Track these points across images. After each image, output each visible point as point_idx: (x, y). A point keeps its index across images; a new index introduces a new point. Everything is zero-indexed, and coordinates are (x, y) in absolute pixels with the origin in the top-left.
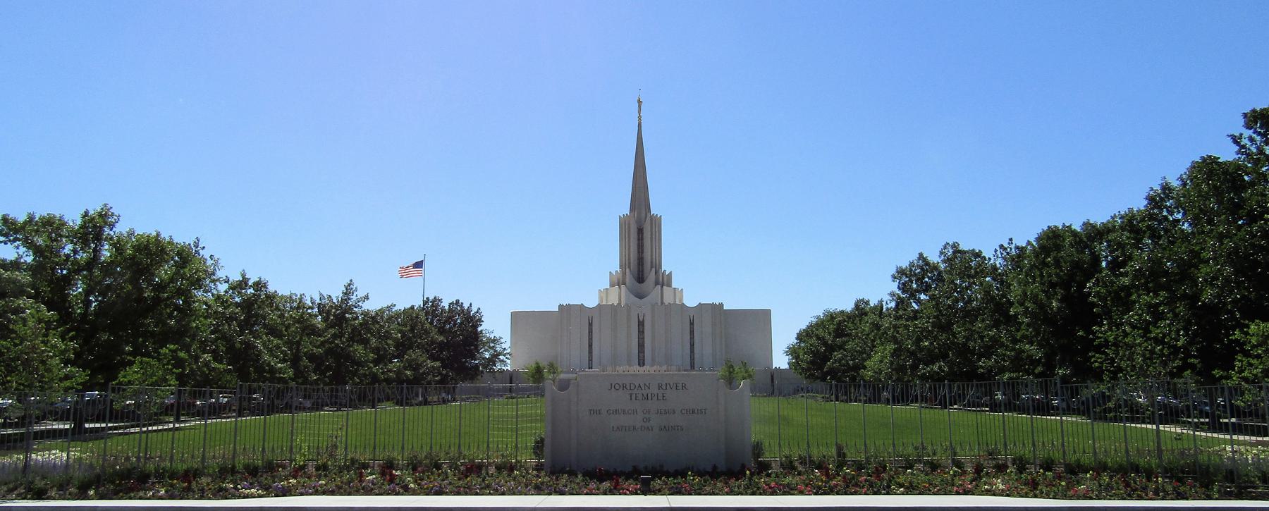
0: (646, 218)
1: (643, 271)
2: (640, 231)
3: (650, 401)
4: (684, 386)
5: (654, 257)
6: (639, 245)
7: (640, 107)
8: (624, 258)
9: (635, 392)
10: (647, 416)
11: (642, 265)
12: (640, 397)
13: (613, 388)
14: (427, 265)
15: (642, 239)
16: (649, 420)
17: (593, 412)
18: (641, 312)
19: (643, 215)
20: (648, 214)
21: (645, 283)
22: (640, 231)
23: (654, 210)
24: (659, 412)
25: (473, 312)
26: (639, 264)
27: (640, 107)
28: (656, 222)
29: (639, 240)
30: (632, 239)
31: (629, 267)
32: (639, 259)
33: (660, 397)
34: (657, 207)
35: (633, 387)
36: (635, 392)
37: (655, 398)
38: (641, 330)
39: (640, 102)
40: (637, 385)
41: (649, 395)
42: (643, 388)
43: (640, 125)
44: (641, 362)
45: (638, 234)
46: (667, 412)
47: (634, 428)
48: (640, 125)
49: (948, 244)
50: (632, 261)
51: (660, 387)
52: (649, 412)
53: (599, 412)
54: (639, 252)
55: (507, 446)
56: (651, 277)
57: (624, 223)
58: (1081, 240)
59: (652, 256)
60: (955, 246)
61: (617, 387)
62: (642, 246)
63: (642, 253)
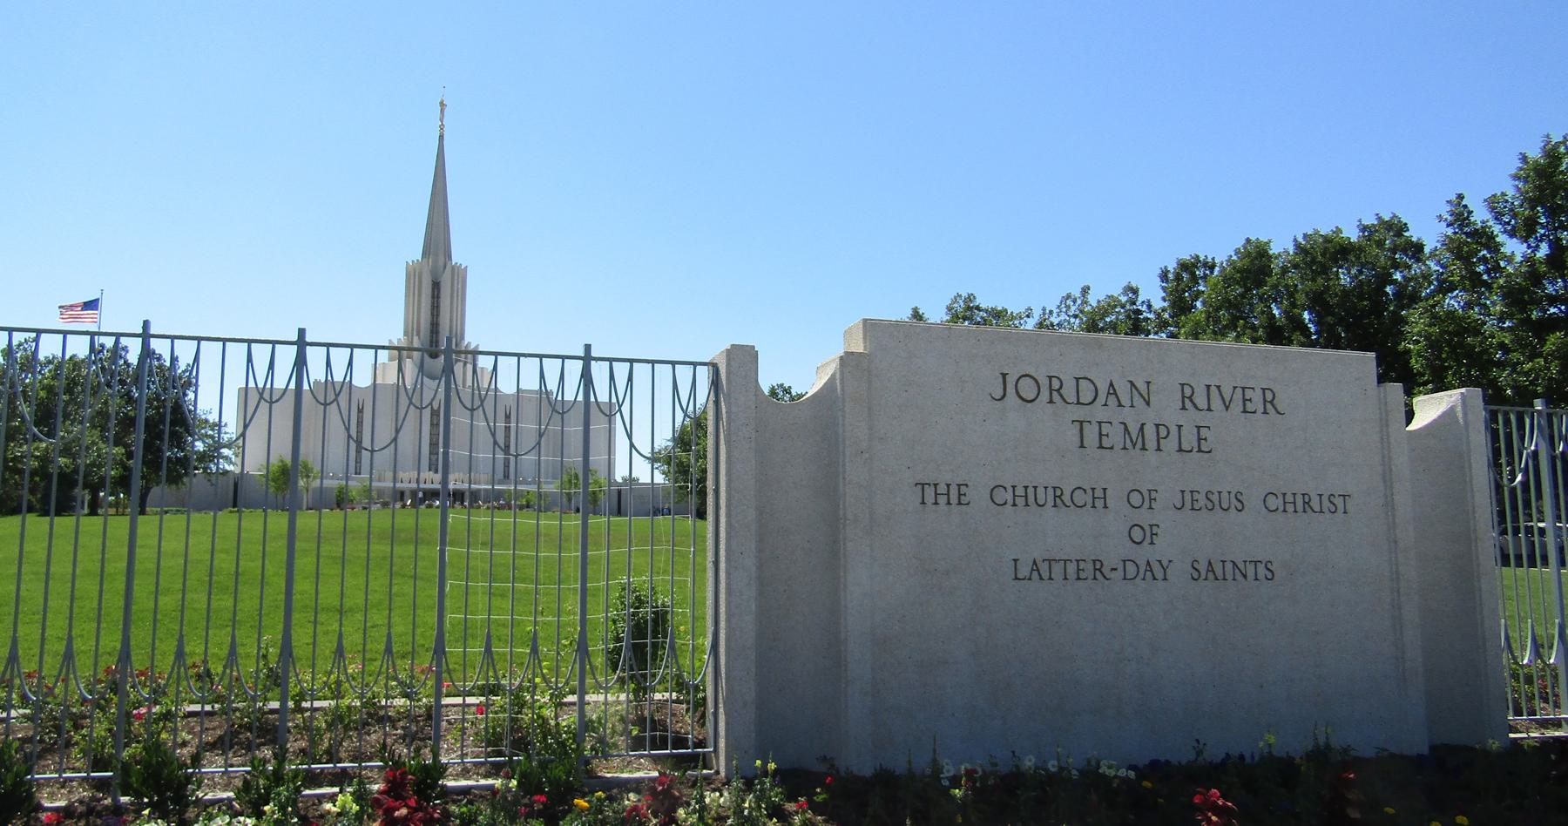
0: (445, 267)
2: (436, 286)
3: (1151, 455)
4: (1270, 401)
5: (454, 327)
6: (433, 306)
7: (442, 111)
8: (411, 317)
9: (1099, 412)
10: (1144, 517)
12: (1115, 436)
13: (1044, 382)
14: (104, 305)
15: (438, 297)
16: (1151, 533)
17: (934, 493)
19: (441, 263)
20: (449, 263)
21: (436, 360)
22: (436, 286)
23: (458, 257)
24: (1189, 502)
25: (179, 371)
26: (432, 332)
27: (442, 111)
28: (459, 275)
29: (433, 297)
30: (423, 296)
31: (418, 334)
32: (432, 324)
33: (1189, 440)
34: (460, 254)
35: (1087, 396)
36: (1099, 412)
37: (1170, 445)
38: (435, 423)
39: (442, 104)
40: (1103, 388)
41: (1150, 431)
42: (1125, 401)
43: (441, 137)
44: (433, 467)
46: (1214, 503)
47: (1098, 567)
48: (441, 137)
49: (960, 296)
50: (422, 321)
51: (1187, 400)
52: (1150, 499)
53: (958, 495)
54: (432, 314)
55: (535, 650)
57: (413, 275)
58: (1314, 261)
59: (451, 320)
60: (970, 298)
61: (1028, 389)
62: (438, 307)
63: (438, 315)
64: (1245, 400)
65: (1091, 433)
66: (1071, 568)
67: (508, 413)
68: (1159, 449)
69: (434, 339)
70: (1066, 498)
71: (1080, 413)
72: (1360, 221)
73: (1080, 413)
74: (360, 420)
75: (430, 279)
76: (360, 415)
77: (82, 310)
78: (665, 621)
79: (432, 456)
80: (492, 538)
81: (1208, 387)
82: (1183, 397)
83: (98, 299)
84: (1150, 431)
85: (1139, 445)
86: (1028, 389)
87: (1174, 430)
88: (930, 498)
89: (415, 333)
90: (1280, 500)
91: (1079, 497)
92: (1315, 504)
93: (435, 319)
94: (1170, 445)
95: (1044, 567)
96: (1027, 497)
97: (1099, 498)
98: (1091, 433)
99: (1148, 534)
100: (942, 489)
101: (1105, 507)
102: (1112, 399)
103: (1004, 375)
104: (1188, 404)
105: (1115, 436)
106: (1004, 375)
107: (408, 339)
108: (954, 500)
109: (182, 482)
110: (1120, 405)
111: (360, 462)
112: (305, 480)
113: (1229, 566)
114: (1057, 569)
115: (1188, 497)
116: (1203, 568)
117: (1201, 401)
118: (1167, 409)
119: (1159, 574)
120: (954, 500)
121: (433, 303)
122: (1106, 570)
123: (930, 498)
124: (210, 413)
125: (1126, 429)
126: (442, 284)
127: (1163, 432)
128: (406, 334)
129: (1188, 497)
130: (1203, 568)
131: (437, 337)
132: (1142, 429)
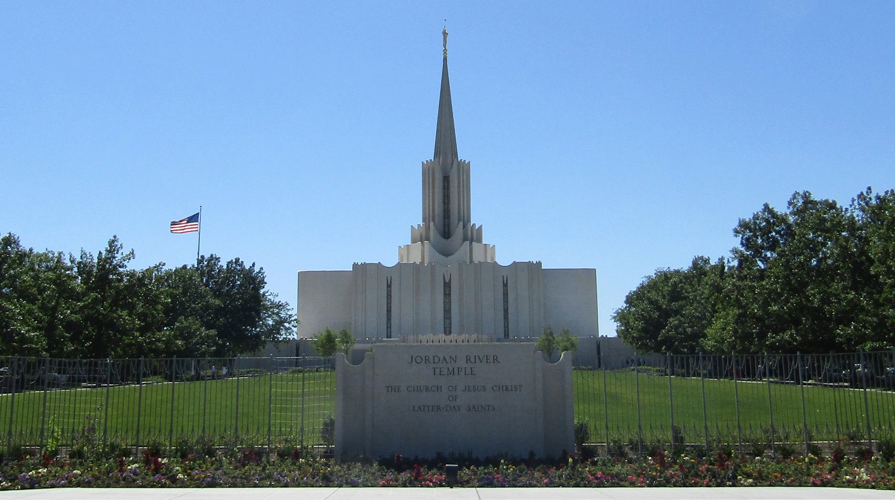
1: (449, 226)
2: (446, 179)
4: (495, 359)
8: (427, 205)
11: (449, 218)
12: (445, 371)
14: (203, 218)
15: (448, 188)
18: (447, 271)
19: (449, 161)
22: (446, 179)
24: (467, 389)
28: (464, 169)
30: (436, 190)
31: (434, 221)
33: (468, 371)
34: (463, 154)
35: (436, 360)
37: (462, 373)
39: (445, 34)
40: (442, 358)
41: (456, 370)
43: (445, 59)
45: (444, 182)
48: (445, 59)
50: (436, 213)
51: (468, 360)
56: (458, 232)
57: (428, 171)
59: (459, 205)
60: (806, 196)
61: (419, 360)
63: (448, 203)
64: (487, 359)
65: (437, 371)
66: (430, 408)
67: (505, 282)
68: (459, 374)
69: (447, 222)
70: (430, 388)
71: (435, 365)
72: (878, 194)
73: (435, 365)
74: (389, 294)
75: (442, 175)
76: (389, 289)
77: (187, 223)
78: (334, 424)
79: (446, 320)
80: (605, 390)
81: (475, 356)
82: (467, 360)
83: (199, 213)
84: (456, 370)
85: (452, 374)
86: (419, 360)
87: (464, 370)
88: (390, 390)
89: (431, 219)
90: (498, 388)
91: (433, 389)
92: (510, 388)
93: (446, 207)
94: (462, 373)
95: (422, 408)
96: (418, 389)
97: (439, 388)
98: (437, 371)
99: (454, 398)
100: (393, 387)
101: (441, 391)
102: (444, 361)
103: (412, 357)
104: (468, 361)
105: (445, 371)
106: (412, 357)
107: (426, 225)
108: (397, 390)
109: (258, 349)
110: (447, 363)
111: (390, 327)
112: (345, 345)
113: (480, 407)
114: (426, 409)
115: (467, 388)
116: (471, 408)
117: (473, 360)
118: (462, 363)
119: (457, 409)
120: (397, 390)
121: (444, 194)
122: (441, 409)
123: (390, 390)
124: (277, 296)
125: (448, 369)
126: (451, 179)
127: (460, 369)
128: (424, 220)
129: (467, 388)
130: (471, 408)
131: (449, 221)
132: (453, 369)
